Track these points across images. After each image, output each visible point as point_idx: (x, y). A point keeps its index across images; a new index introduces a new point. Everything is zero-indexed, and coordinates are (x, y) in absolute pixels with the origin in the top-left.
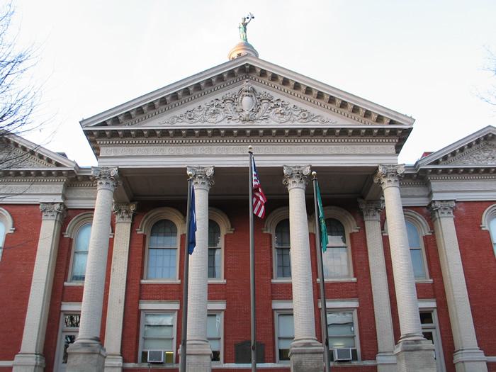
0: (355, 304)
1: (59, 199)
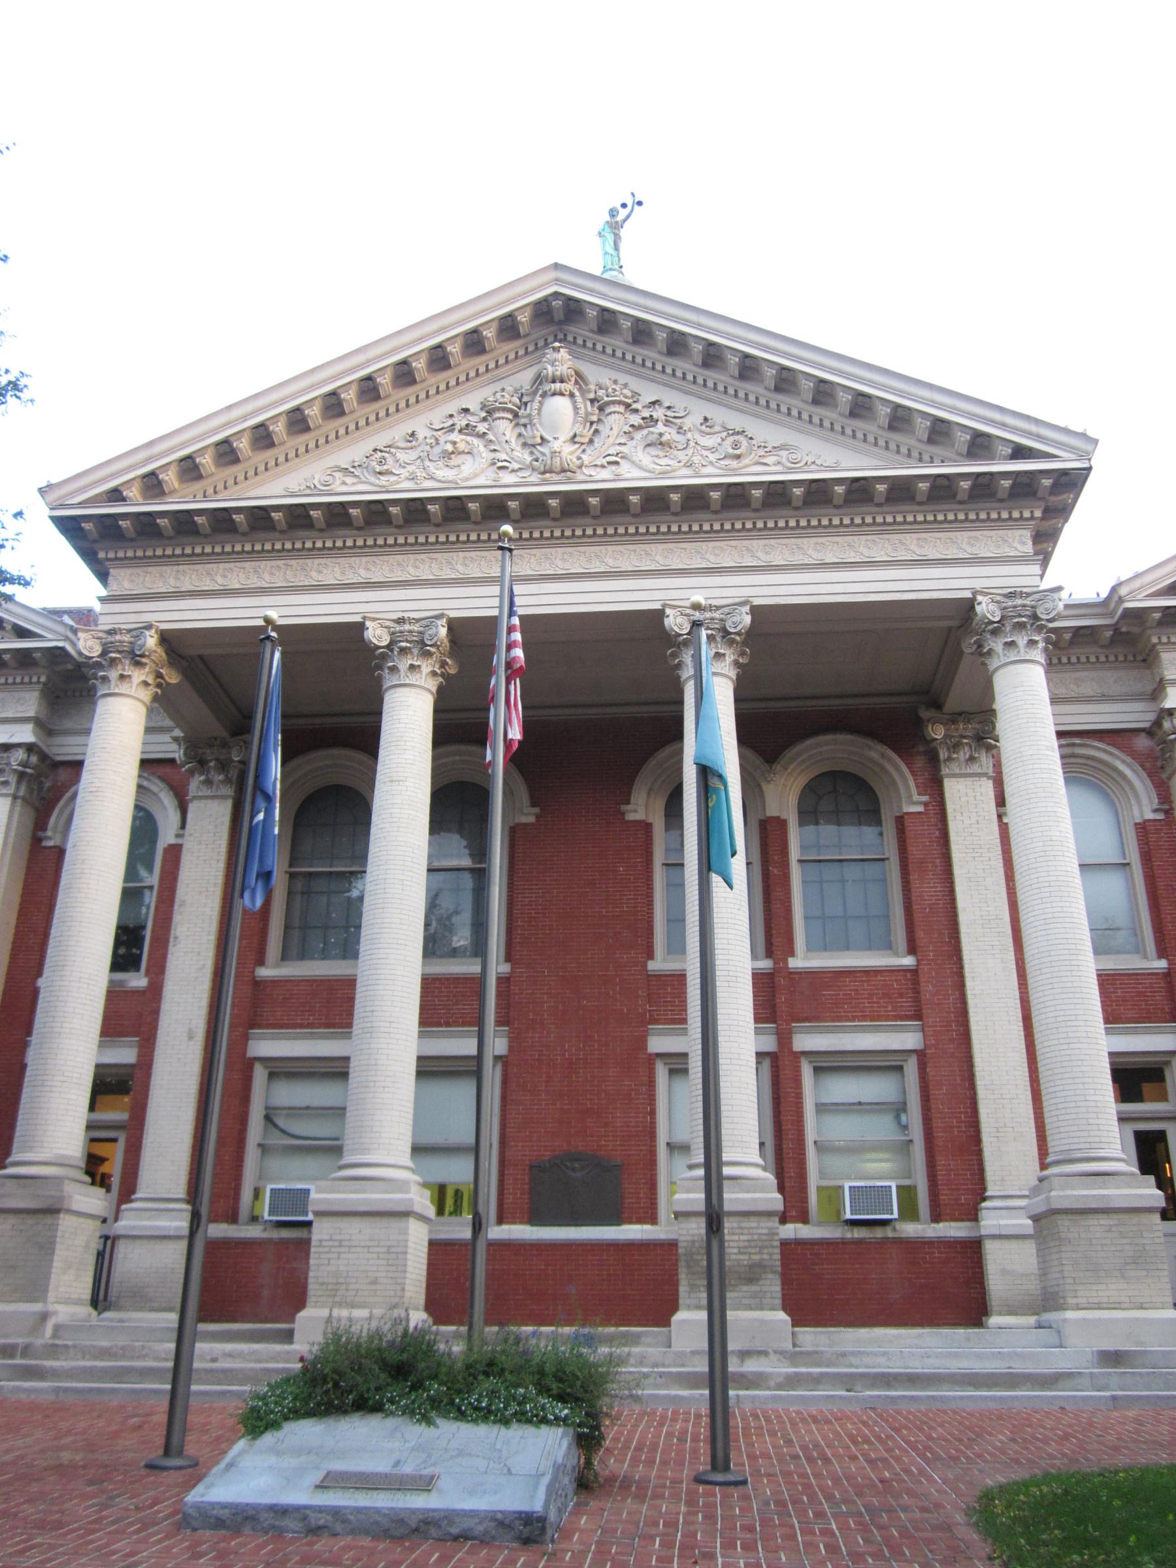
0: (907, 1039)
1: (25, 734)
